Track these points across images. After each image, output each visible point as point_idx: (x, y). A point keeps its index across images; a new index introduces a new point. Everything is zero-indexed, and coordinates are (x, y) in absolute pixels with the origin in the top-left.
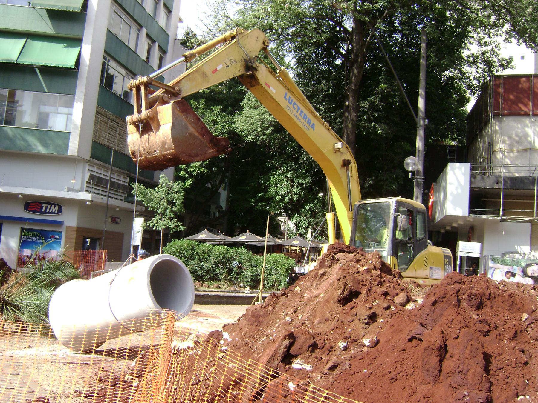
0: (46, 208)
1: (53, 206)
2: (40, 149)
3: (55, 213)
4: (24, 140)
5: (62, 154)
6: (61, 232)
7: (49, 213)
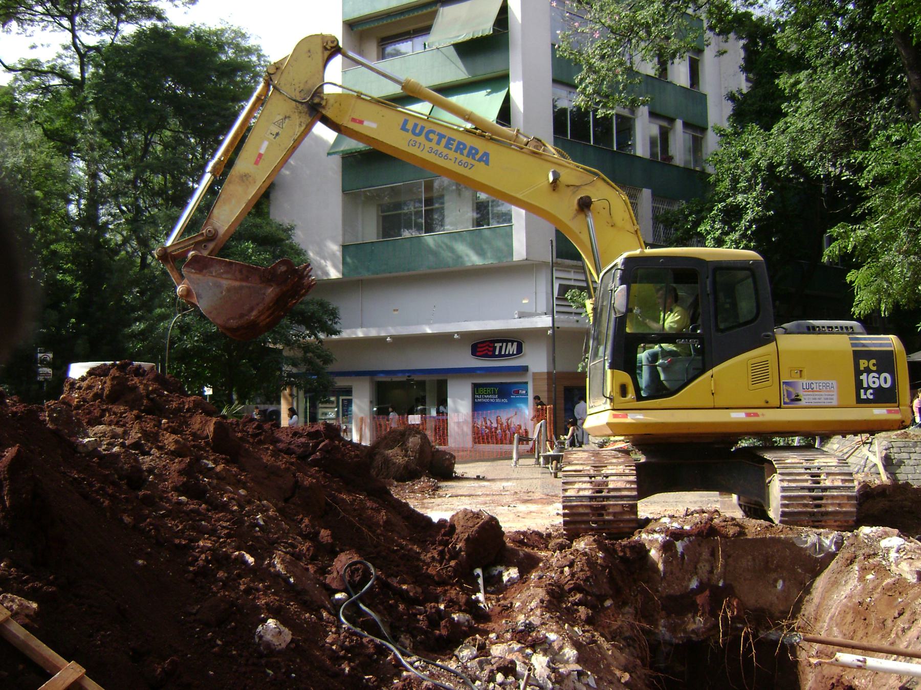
0: (501, 348)
1: (510, 344)
2: (474, 259)
3: (513, 355)
4: (452, 250)
5: (505, 262)
6: (526, 383)
7: (505, 355)
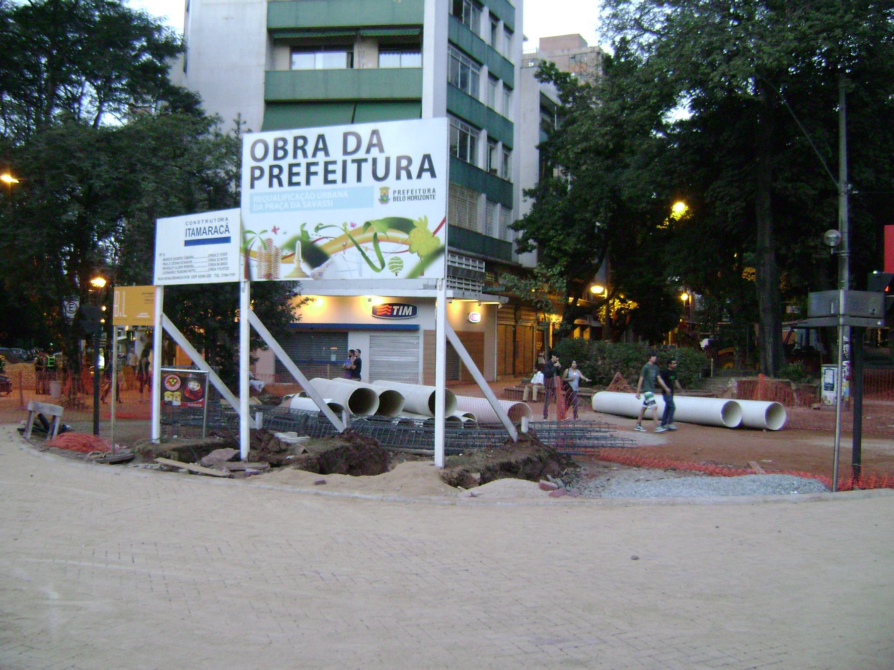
0: (398, 310)
1: (406, 308)
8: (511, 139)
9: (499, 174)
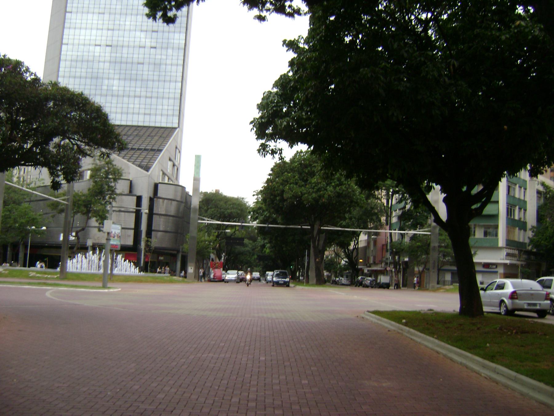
8: (526, 207)
9: (522, 220)
